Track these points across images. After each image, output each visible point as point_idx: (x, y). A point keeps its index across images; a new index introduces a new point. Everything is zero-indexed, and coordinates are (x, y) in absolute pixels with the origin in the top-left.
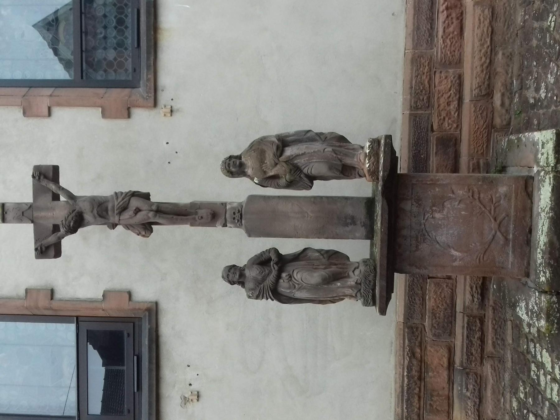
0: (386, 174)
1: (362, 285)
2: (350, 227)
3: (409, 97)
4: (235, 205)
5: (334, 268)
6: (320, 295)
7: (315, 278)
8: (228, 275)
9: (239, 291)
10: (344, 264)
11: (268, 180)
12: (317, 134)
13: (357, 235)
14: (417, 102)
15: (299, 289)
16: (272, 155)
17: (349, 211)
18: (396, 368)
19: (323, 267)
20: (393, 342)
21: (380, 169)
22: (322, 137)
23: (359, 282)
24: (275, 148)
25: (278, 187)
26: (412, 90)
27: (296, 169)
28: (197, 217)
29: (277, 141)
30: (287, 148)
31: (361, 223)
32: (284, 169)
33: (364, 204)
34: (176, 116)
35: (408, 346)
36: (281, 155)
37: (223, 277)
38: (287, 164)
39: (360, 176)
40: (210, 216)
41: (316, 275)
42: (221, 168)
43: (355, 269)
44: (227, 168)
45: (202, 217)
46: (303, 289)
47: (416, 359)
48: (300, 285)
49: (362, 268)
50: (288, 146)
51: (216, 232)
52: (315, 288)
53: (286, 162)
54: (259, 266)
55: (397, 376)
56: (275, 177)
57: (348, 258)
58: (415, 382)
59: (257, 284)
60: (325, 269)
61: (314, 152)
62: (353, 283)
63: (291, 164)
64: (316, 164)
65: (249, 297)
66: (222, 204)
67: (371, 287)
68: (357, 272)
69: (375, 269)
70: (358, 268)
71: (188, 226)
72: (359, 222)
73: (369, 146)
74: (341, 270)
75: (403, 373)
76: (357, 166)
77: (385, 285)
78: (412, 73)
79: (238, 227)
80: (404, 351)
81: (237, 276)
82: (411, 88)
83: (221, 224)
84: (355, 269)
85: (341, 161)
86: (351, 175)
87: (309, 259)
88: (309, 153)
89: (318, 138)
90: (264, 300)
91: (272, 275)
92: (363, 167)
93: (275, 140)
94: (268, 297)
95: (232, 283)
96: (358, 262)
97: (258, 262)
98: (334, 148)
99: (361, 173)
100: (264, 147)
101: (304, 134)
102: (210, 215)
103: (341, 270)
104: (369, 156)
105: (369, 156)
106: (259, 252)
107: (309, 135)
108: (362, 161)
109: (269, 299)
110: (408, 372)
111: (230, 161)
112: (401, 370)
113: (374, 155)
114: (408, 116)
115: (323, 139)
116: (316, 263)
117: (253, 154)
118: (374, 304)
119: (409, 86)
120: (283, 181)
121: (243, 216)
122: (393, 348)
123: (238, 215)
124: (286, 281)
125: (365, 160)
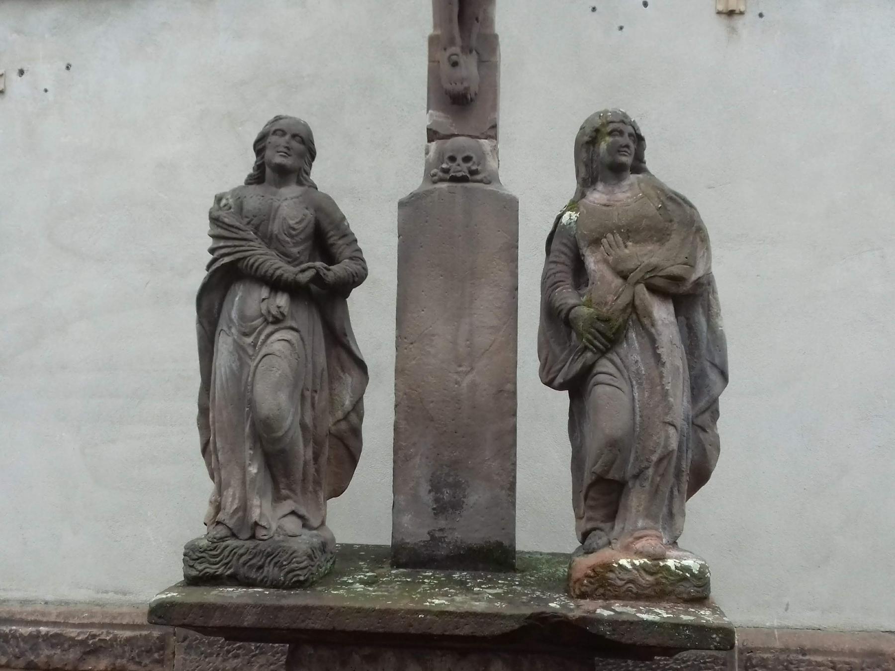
0: (606, 630)
1: (250, 544)
2: (428, 498)
3: (778, 645)
4: (491, 163)
5: (303, 452)
6: (220, 415)
7: (273, 396)
8: (284, 133)
9: (232, 167)
10: (317, 483)
11: (568, 253)
12: (715, 401)
13: (406, 519)
15: (239, 348)
16: (654, 260)
17: (477, 496)
18: (61, 603)
19: (308, 420)
20: (128, 597)
21: (618, 606)
22: (707, 416)
23: (260, 533)
24: (676, 270)
25: (549, 285)
27: (609, 336)
28: (456, 49)
29: (694, 277)
30: (671, 308)
31: (441, 530)
32: (610, 298)
34: (719, 26)
35: (115, 638)
36: (654, 290)
37: (278, 119)
38: (624, 310)
39: (585, 536)
40: (459, 88)
41: (283, 397)
42: (606, 112)
43: (301, 517)
45: (455, 64)
46: (240, 359)
47: (81, 659)
48: (251, 352)
49: (304, 541)
50: (677, 314)
51: (412, 110)
52: (244, 398)
53: (632, 306)
54: (310, 230)
55: (39, 607)
56: (579, 273)
57: (337, 492)
58: (23, 654)
59: (255, 221)
60: (303, 427)
61: (665, 394)
62: (255, 515)
63: (626, 321)
64: (626, 399)
65: (219, 199)
66: (494, 127)
67: (243, 571)
68: (292, 525)
69: (299, 585)
70: (306, 525)
71: (427, 27)
72: (442, 523)
73: (688, 569)
74: (299, 475)
75: (46, 624)
76: (618, 527)
77: (245, 624)
78: (841, 653)
79: (427, 171)
80: (102, 626)
81: (278, 160)
83: (435, 122)
84: (301, 517)
85: (636, 477)
86: (591, 508)
87: (333, 378)
88: (661, 377)
89: (702, 404)
90: (210, 242)
91: (281, 264)
92: (617, 545)
93: (699, 272)
94: (217, 254)
95: (260, 146)
96: (323, 523)
97: (325, 224)
99: (596, 539)
100: (675, 239)
101: (717, 361)
102: (462, 98)
103: (299, 475)
104: (656, 568)
105: (656, 568)
106: (353, 229)
108: (639, 545)
109: (210, 257)
110: (47, 638)
111: (630, 135)
112: (53, 619)
113: (658, 583)
115: (699, 421)
116: (322, 399)
117: (652, 208)
118: (192, 581)
119: (808, 645)
121: (459, 185)
122: (110, 596)
123: (462, 169)
124: (264, 306)
125: (640, 554)
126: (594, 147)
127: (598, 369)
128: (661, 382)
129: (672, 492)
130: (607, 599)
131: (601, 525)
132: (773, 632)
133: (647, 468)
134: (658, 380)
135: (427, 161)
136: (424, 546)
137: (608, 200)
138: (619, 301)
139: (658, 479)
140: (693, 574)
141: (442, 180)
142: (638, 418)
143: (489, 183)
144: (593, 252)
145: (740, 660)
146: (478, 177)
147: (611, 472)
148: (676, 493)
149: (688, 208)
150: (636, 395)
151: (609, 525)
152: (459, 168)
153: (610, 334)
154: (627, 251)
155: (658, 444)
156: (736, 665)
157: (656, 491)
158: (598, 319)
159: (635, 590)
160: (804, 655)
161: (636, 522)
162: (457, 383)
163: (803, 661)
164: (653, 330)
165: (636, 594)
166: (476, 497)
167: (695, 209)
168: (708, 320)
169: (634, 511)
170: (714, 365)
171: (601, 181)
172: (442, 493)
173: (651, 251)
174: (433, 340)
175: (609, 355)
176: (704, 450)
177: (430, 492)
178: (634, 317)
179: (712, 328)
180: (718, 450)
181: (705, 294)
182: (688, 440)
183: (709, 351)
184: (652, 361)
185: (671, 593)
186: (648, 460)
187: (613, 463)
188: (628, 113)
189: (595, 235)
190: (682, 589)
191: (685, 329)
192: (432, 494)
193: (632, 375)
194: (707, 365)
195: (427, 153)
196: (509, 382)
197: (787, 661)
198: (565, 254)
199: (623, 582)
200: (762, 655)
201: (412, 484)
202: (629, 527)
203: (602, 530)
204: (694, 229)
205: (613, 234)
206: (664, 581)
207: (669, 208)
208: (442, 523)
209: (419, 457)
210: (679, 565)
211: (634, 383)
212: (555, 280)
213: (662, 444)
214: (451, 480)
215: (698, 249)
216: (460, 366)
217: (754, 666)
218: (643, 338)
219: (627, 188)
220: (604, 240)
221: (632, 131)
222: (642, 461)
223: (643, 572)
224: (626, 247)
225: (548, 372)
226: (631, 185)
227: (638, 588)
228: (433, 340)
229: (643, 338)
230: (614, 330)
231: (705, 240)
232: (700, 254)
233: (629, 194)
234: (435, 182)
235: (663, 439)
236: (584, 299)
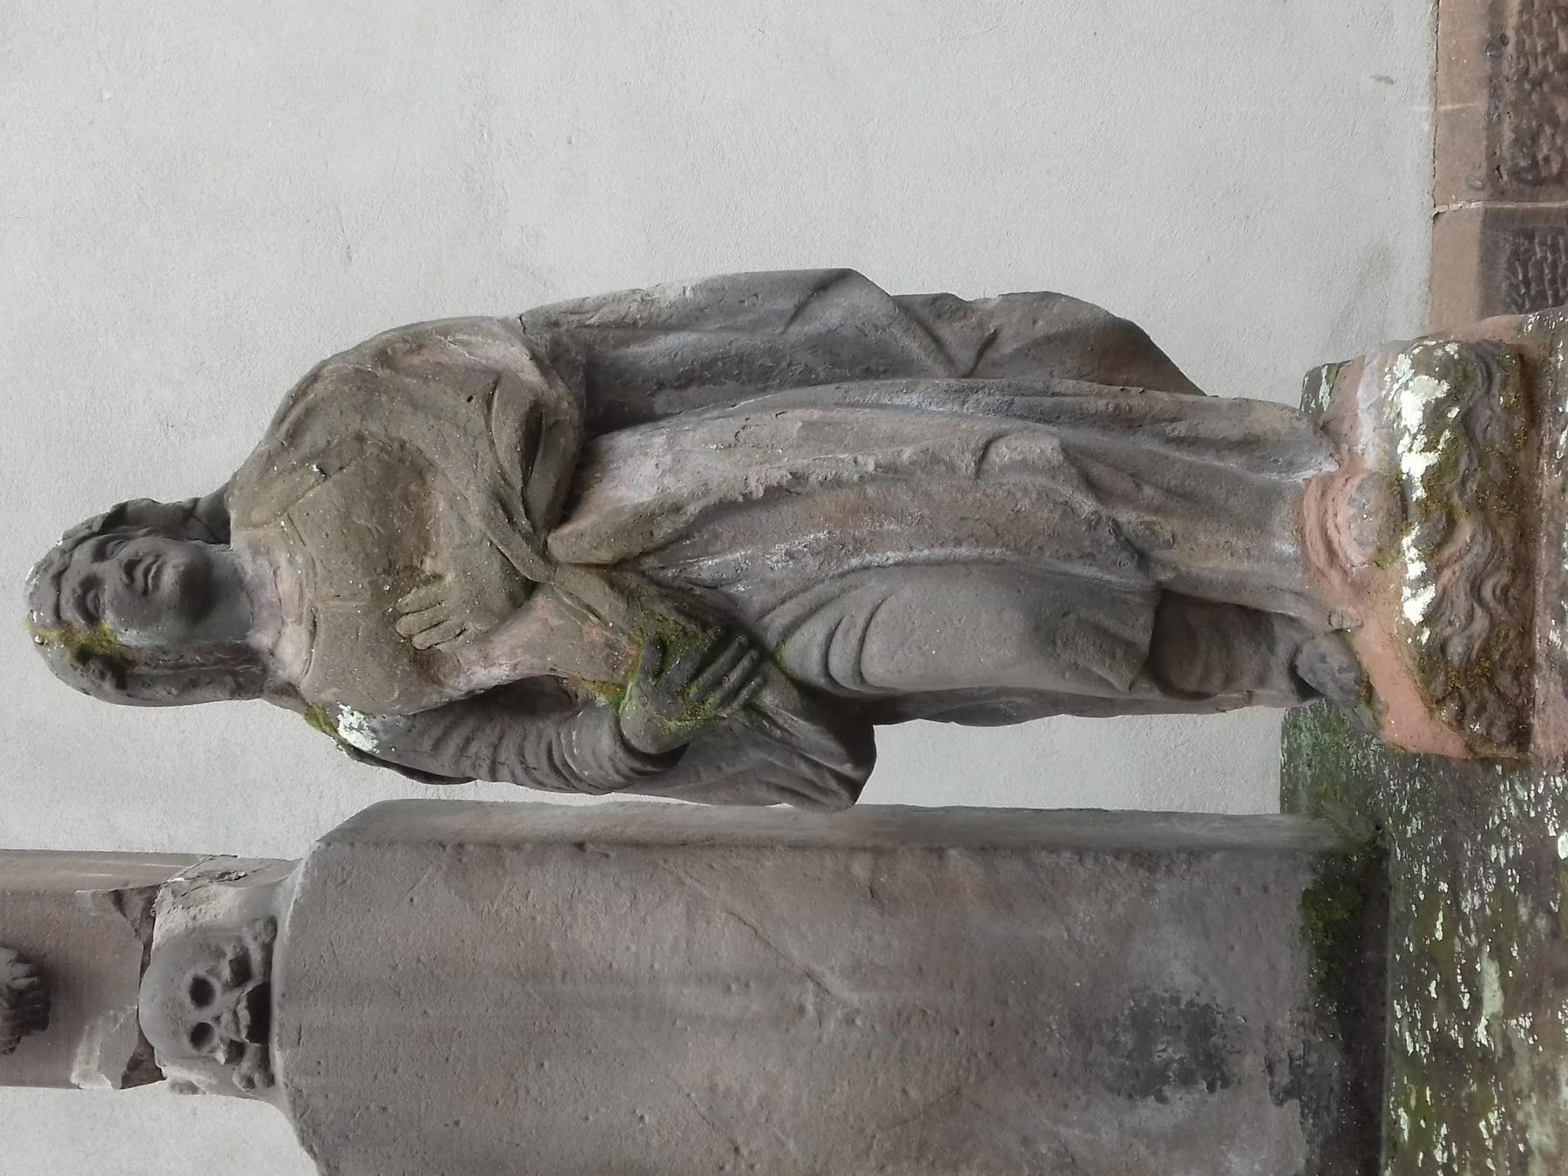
2: (1181, 1105)
12: (905, 307)
14: (1535, 137)
16: (476, 503)
17: (1175, 963)
22: (946, 332)
24: (506, 433)
26: (1497, 58)
27: (713, 640)
29: (531, 375)
30: (625, 440)
31: (1270, 1068)
32: (595, 634)
33: (1293, 915)
36: (568, 503)
38: (630, 596)
44: (79, 622)
50: (640, 417)
53: (613, 572)
61: (891, 472)
63: (668, 591)
64: (908, 592)
72: (1250, 1064)
73: (1434, 414)
82: (1497, 42)
83: (104, 1067)
85: (1142, 559)
88: (838, 483)
89: (913, 345)
93: (514, 356)
98: (1068, 433)
100: (415, 431)
101: (786, 304)
107: (832, 313)
108: (1355, 556)
111: (100, 555)
113: (1479, 506)
114: (1474, 228)
115: (966, 356)
117: (321, 496)
119: (1478, 31)
120: (591, 742)
121: (276, 1013)
123: (229, 1006)
125: (1385, 553)
126: (133, 663)
127: (813, 672)
128: (852, 486)
129: (1179, 442)
130: (1531, 661)
131: (1282, 651)
132: (1447, 114)
133: (1117, 527)
134: (850, 496)
135: (211, 1088)
136: (1316, 1115)
137: (299, 621)
138: (604, 610)
139: (1148, 491)
140: (1453, 397)
141: (265, 1062)
142: (963, 551)
143: (273, 923)
144: (458, 668)
145: (1519, 196)
146: (256, 956)
147: (1128, 634)
148: (1181, 429)
149: (319, 386)
150: (893, 556)
151: (1279, 630)
152: (226, 1017)
153: (705, 640)
154: (450, 578)
155: (1044, 495)
156: (1529, 205)
157: (1185, 496)
158: (658, 675)
159: (1504, 578)
160: (1504, 40)
161: (1281, 560)
162: (850, 1021)
163: (1520, 43)
164: (693, 509)
165: (1514, 572)
166: (1176, 967)
167: (324, 364)
168: (667, 328)
169: (1246, 566)
170: (798, 311)
171: (245, 637)
172: (1167, 1064)
173: (452, 505)
174: (728, 1089)
175: (771, 638)
176: (1048, 339)
177: (1162, 1099)
178: (650, 563)
179: (687, 317)
180: (1047, 296)
181: (587, 335)
182: (1019, 391)
183: (755, 326)
184: (788, 512)
185: (1509, 466)
186: (1093, 524)
187: (1101, 632)
188: (40, 556)
189: (403, 666)
190: (1496, 433)
191: (692, 391)
192: (1167, 1091)
193: (834, 570)
194: (800, 331)
195: (193, 1089)
196: (847, 868)
197: (1519, 81)
198: (468, 741)
199: (1479, 612)
200: (1506, 144)
201: (1142, 1149)
202: (1294, 578)
203: (1297, 650)
204: (382, 373)
205: (396, 616)
206: (1473, 486)
207: (322, 443)
208: (1250, 1064)
209: (1063, 1131)
210: (1422, 440)
211: (854, 562)
212: (545, 767)
213: (1042, 481)
214: (1127, 1039)
215: (445, 359)
216: (802, 1010)
217: (1535, 163)
218: (716, 536)
219: (262, 561)
220: (419, 641)
221: (87, 548)
222: (1096, 543)
223: (1447, 553)
224: (438, 577)
225: (824, 791)
226: (255, 550)
227: (1497, 568)
228: (728, 1089)
229: (716, 536)
230: (692, 627)
231: (416, 338)
232: (458, 354)
233: (282, 558)
234: (270, 1080)
235: (1026, 479)
236: (602, 700)
